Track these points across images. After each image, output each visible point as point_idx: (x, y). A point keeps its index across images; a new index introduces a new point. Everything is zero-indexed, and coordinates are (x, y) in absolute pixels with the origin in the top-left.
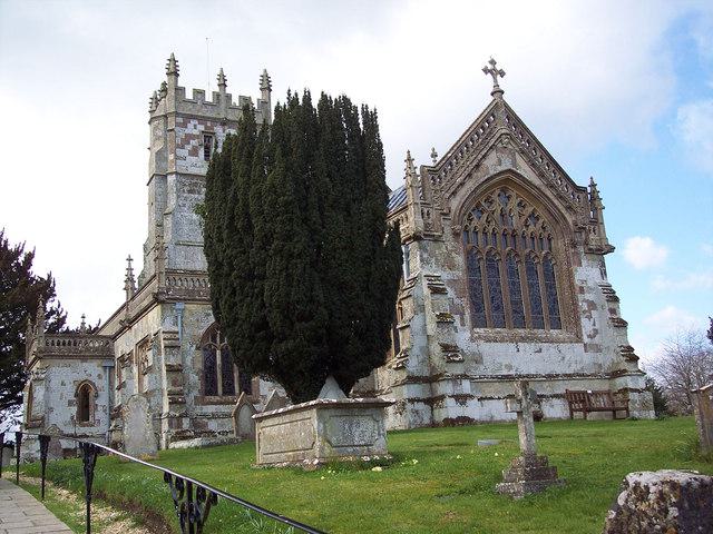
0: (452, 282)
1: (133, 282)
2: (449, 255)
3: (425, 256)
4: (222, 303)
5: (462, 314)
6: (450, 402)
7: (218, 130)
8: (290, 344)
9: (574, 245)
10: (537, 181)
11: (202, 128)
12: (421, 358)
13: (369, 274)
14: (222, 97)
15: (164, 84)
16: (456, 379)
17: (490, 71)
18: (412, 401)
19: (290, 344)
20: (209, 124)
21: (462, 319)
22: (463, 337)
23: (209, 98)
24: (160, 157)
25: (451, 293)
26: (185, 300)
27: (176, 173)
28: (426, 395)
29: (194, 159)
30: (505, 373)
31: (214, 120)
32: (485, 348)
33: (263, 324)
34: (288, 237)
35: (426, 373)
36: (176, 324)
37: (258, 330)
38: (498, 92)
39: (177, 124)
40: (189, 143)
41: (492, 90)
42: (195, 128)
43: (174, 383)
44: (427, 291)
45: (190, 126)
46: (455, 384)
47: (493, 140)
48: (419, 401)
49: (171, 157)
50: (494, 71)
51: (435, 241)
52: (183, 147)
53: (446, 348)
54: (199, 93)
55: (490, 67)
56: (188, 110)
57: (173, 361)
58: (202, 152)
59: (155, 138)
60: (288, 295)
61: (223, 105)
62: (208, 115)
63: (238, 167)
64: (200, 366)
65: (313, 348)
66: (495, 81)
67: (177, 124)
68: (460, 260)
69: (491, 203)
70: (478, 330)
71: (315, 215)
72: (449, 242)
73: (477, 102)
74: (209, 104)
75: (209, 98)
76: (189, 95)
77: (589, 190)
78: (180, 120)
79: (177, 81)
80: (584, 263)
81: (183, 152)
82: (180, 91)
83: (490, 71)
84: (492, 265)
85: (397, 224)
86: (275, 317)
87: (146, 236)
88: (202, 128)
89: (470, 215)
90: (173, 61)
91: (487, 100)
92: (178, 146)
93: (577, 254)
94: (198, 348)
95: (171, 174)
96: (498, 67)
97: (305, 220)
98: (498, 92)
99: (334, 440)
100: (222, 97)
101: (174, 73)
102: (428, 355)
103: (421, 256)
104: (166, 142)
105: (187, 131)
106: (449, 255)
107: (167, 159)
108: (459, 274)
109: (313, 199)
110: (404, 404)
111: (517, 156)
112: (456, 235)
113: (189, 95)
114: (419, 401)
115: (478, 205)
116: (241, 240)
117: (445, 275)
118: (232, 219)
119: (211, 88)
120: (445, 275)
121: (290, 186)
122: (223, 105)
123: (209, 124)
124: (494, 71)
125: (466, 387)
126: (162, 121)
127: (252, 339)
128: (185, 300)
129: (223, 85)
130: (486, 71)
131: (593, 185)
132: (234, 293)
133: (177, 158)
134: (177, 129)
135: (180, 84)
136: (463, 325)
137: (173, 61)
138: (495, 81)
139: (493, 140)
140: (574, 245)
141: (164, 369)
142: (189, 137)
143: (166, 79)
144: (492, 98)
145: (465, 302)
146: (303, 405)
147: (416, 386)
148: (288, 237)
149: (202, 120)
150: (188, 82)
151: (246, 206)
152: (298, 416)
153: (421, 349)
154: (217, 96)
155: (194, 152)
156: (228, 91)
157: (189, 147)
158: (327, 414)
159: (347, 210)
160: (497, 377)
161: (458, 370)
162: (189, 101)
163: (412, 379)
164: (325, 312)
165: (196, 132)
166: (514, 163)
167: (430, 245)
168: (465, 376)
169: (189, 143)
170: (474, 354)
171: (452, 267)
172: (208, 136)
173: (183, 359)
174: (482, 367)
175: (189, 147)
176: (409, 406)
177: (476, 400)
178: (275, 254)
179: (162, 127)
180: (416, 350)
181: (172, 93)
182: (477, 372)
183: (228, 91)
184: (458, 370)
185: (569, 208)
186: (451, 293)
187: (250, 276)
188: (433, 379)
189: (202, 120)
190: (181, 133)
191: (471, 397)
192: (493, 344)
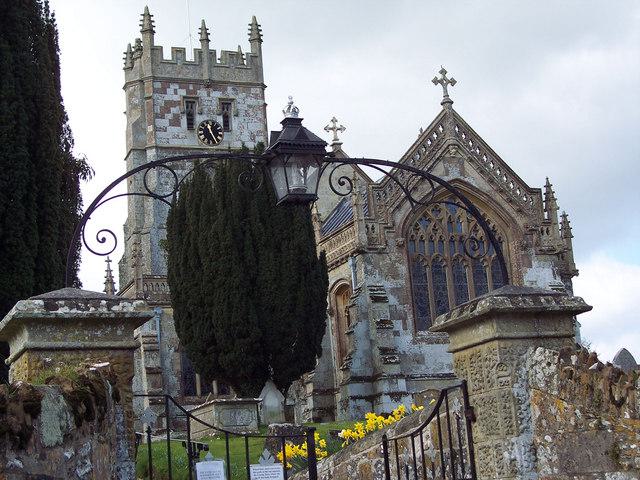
0: (394, 291)
1: (113, 283)
2: (393, 265)
3: (369, 267)
4: (181, 323)
5: (404, 320)
6: (385, 399)
7: (202, 93)
8: (232, 356)
9: (525, 248)
10: (486, 187)
11: (183, 92)
12: (364, 360)
13: (295, 299)
14: (205, 54)
15: (138, 41)
16: (393, 378)
17: (441, 82)
18: (354, 398)
19: (232, 356)
20: (191, 88)
21: (404, 324)
22: (405, 342)
23: (190, 57)
24: (136, 129)
25: (392, 300)
26: (162, 304)
27: (157, 147)
28: (369, 393)
29: (175, 130)
30: (447, 371)
31: (198, 83)
32: (426, 349)
33: (213, 341)
34: (229, 273)
35: (369, 373)
36: (154, 328)
37: (209, 345)
38: (447, 102)
39: (155, 91)
40: (169, 112)
41: (442, 99)
42: (176, 94)
43: (154, 385)
44: (369, 300)
45: (170, 91)
46: (391, 383)
47: (440, 151)
48: (361, 398)
49: (150, 129)
50: (444, 81)
51: (380, 253)
52: (163, 117)
53: (384, 351)
54: (179, 52)
55: (440, 77)
56: (167, 73)
57: (152, 364)
58: (184, 121)
59: (131, 106)
60: (229, 318)
61: (205, 65)
62: (190, 76)
63: (190, 215)
64: (178, 367)
65: (250, 358)
66: (446, 91)
67: (155, 91)
68: (403, 269)
69: (439, 211)
70: (422, 333)
71: (249, 254)
72: (394, 254)
73: (428, 112)
74: (190, 64)
75: (190, 57)
76: (167, 55)
77: (544, 191)
78: (158, 85)
79: (152, 40)
80: (535, 264)
81: (163, 123)
82: (157, 51)
83: (441, 82)
84: (438, 270)
85: (323, 254)
86: (220, 334)
87: (125, 216)
88: (183, 92)
89: (417, 225)
90: (147, 16)
91: (433, 111)
92: (157, 116)
93: (528, 256)
94: (175, 351)
95: (150, 148)
96: (449, 76)
97: (243, 258)
98: (447, 102)
99: (224, 422)
100: (205, 54)
101: (149, 30)
102: (371, 357)
103: (365, 268)
104: (143, 111)
105: (167, 97)
106: (393, 265)
107: (145, 130)
108: (402, 282)
109: (247, 243)
110: (347, 401)
111: (466, 164)
112: (400, 246)
113: (167, 55)
114: (361, 398)
115: (425, 215)
116: (193, 275)
117: (388, 284)
118: (186, 259)
119: (191, 45)
120: (388, 284)
121: (229, 234)
122: (205, 65)
123: (191, 88)
124: (444, 81)
125: (402, 385)
126: (138, 86)
127: (204, 353)
128: (162, 304)
129: (205, 40)
130: (436, 81)
131: (548, 186)
132: (190, 315)
133: (156, 129)
134: (156, 96)
135: (156, 43)
136: (405, 329)
137: (147, 16)
138: (446, 91)
139: (440, 151)
140: (525, 248)
141: (144, 374)
142: (169, 104)
143: (140, 36)
144: (442, 108)
145: (407, 308)
146: (248, 399)
147: (358, 384)
148: (229, 273)
149: (184, 83)
150: (165, 40)
151: (196, 249)
152: (206, 409)
153: (364, 352)
154: (199, 53)
155: (175, 122)
156: (212, 46)
157: (169, 116)
158: (221, 408)
159: (278, 249)
160: (438, 376)
161: (395, 369)
162: (168, 62)
163: (355, 379)
164: (259, 330)
165: (176, 98)
166: (463, 172)
167: (373, 257)
168: (401, 376)
169: (169, 112)
170: (416, 355)
171: (395, 276)
172: (190, 103)
173: (162, 362)
174: (423, 367)
175: (169, 116)
176: (351, 403)
177: (410, 396)
178: (220, 286)
179: (138, 93)
180: (359, 353)
181: (147, 54)
182: (419, 371)
183: (212, 46)
184: (395, 369)
185: (520, 211)
186: (392, 300)
187: (202, 304)
188: (374, 379)
189: (184, 83)
190: (161, 100)
191: (406, 394)
192: (435, 345)
